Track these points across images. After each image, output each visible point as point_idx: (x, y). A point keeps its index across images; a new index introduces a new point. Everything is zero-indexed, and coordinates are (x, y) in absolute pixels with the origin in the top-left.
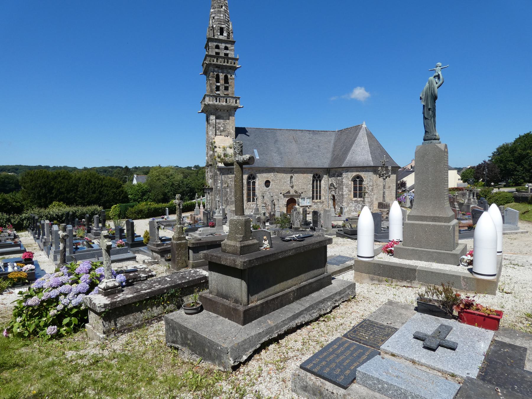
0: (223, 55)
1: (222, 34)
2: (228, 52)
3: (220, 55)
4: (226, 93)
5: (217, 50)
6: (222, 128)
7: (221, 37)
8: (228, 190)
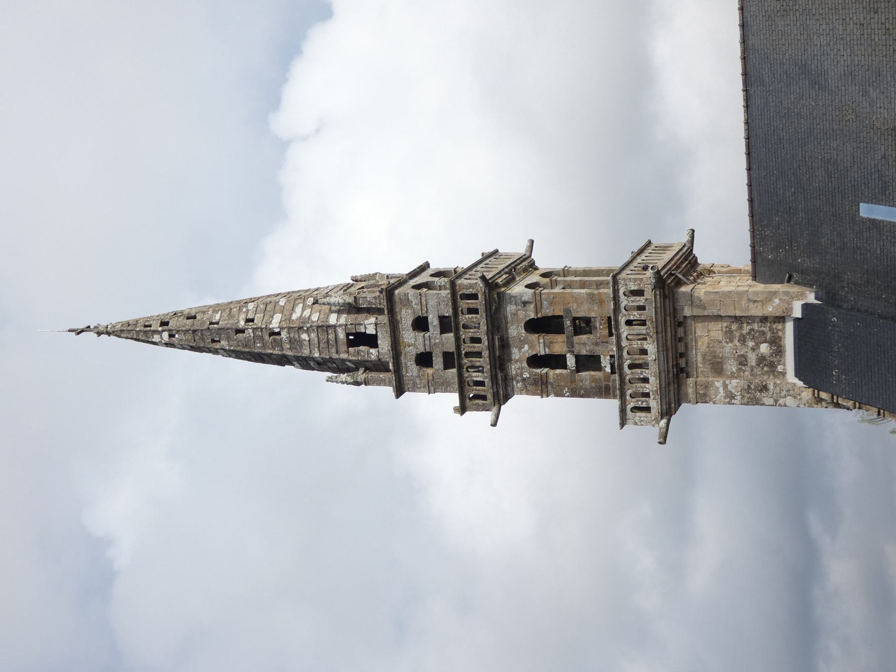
0: (451, 336)
1: (371, 341)
2: (433, 321)
3: (452, 348)
4: (601, 330)
5: (438, 361)
6: (764, 348)
7: (384, 343)
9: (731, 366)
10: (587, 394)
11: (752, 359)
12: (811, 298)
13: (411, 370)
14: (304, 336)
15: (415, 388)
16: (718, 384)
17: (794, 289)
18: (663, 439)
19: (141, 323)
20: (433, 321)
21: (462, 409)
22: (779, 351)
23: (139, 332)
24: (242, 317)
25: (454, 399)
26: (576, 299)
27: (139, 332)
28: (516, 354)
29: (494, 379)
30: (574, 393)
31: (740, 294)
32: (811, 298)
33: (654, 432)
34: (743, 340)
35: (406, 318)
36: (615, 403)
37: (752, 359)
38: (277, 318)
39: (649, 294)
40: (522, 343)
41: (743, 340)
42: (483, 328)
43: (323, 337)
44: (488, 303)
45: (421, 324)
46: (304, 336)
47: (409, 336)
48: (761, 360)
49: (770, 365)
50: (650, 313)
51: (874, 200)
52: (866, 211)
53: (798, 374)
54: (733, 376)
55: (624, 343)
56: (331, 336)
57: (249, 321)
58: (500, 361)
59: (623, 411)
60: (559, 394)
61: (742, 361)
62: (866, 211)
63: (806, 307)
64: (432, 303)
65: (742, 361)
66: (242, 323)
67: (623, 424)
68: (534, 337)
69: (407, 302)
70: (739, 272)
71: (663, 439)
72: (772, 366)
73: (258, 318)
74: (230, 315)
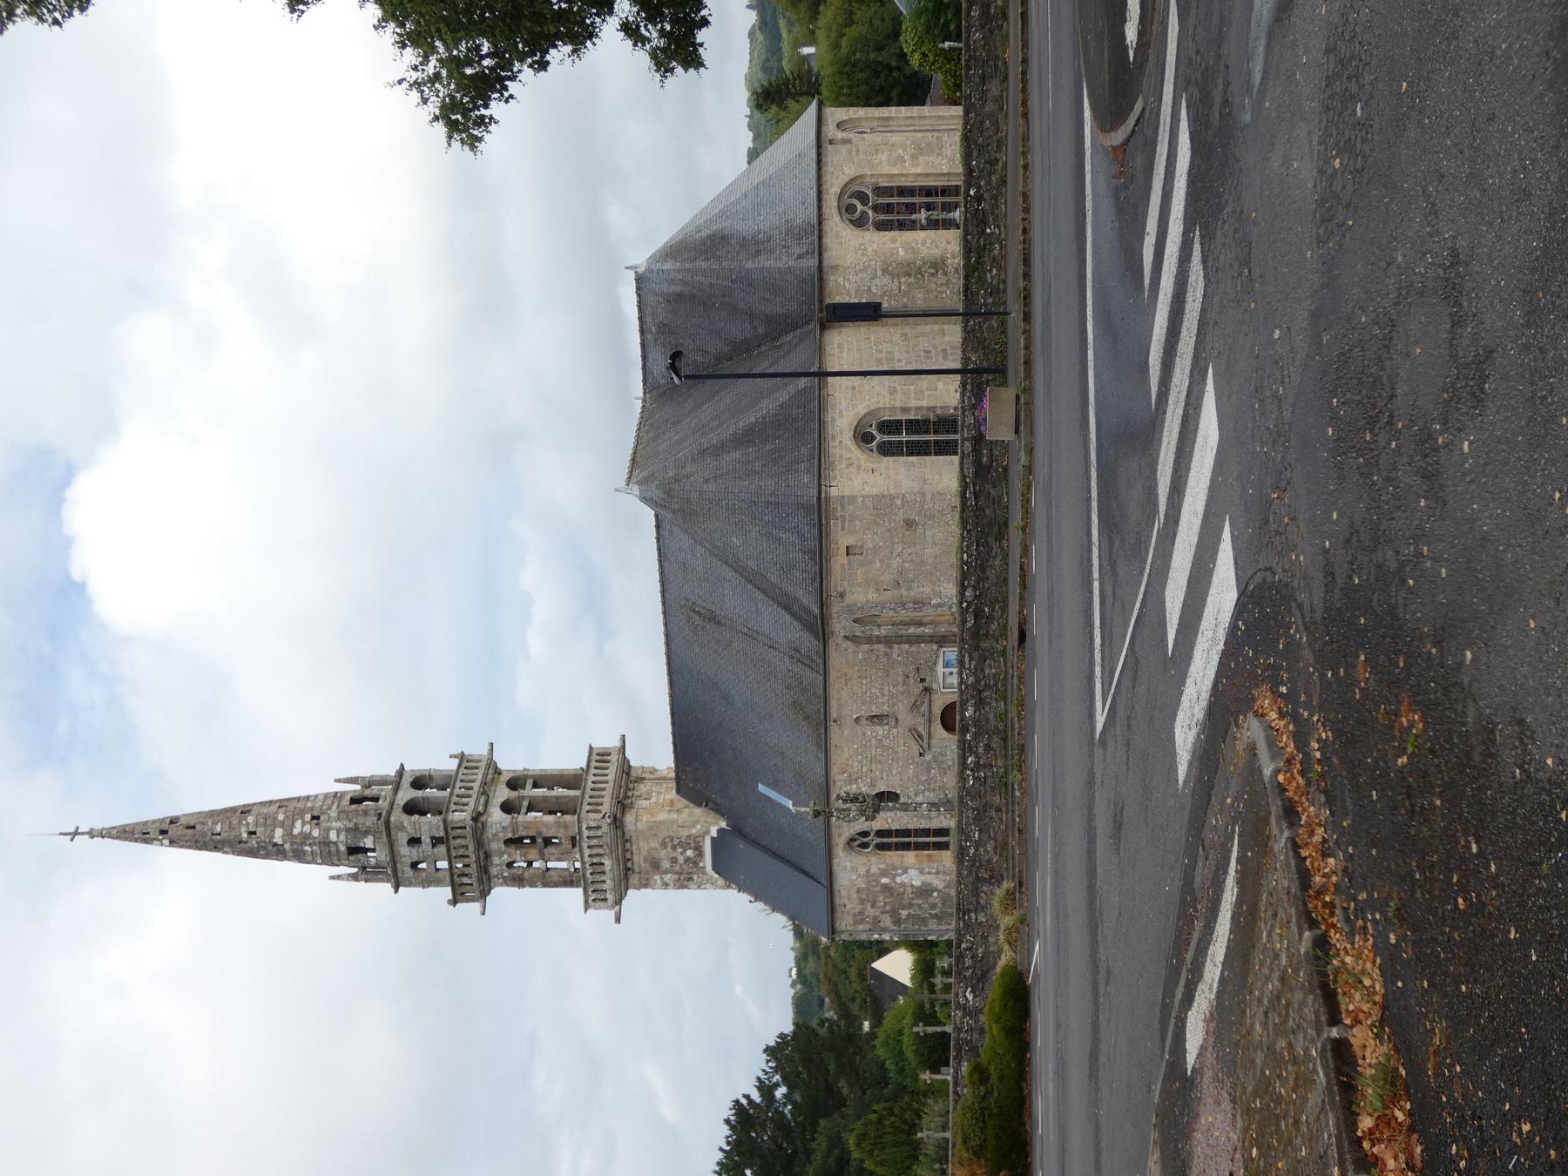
2: (426, 839)
8: (904, 913)
9: (666, 865)
10: (556, 885)
11: (681, 859)
12: (723, 824)
13: (409, 872)
14: (307, 848)
15: (410, 884)
16: (657, 877)
17: (712, 816)
18: (618, 920)
19: (138, 829)
20: (426, 839)
21: (454, 902)
22: (701, 854)
23: (128, 833)
24: (243, 829)
25: (446, 892)
26: (546, 825)
27: (128, 833)
28: (496, 860)
29: (480, 881)
30: (545, 885)
31: (672, 823)
32: (723, 824)
33: (611, 914)
34: (674, 848)
35: (402, 838)
36: (580, 890)
37: (681, 859)
38: (279, 833)
39: (605, 829)
40: (501, 854)
41: (674, 848)
42: (471, 848)
43: (326, 850)
44: (475, 830)
45: (414, 841)
46: (307, 848)
47: (405, 851)
48: (688, 860)
49: (694, 863)
50: (607, 839)
51: (768, 785)
52: (762, 788)
53: (714, 868)
54: (666, 872)
55: (587, 859)
56: (333, 849)
57: (251, 833)
58: (484, 870)
59: (586, 902)
60: (533, 885)
61: (674, 861)
62: (762, 788)
63: (720, 831)
64: (425, 828)
65: (674, 861)
66: (245, 835)
67: (587, 907)
68: (512, 850)
69: (402, 828)
70: (664, 779)
71: (618, 920)
72: (696, 864)
73: (260, 830)
74: (231, 828)
